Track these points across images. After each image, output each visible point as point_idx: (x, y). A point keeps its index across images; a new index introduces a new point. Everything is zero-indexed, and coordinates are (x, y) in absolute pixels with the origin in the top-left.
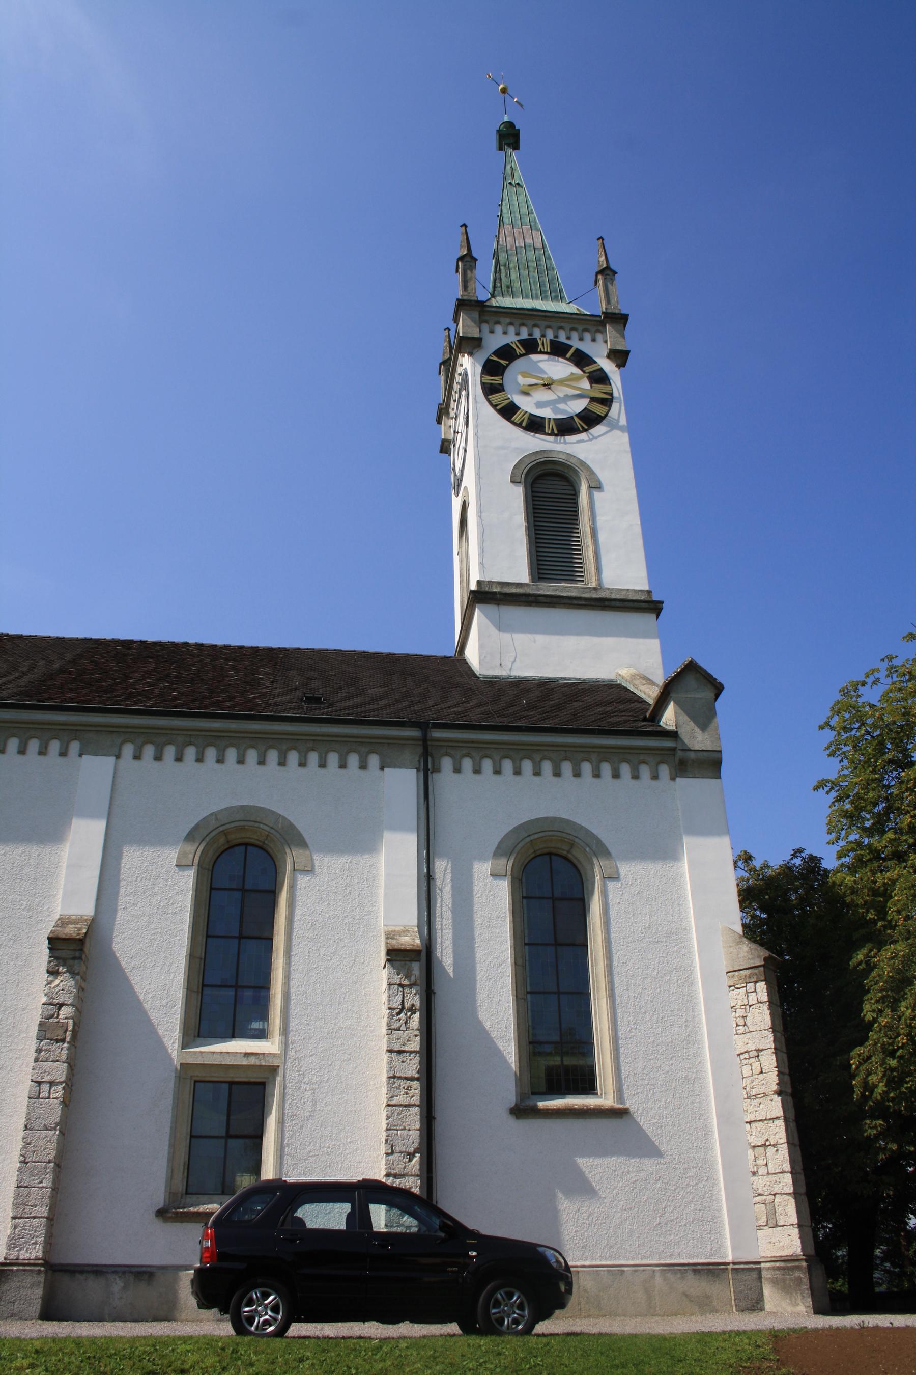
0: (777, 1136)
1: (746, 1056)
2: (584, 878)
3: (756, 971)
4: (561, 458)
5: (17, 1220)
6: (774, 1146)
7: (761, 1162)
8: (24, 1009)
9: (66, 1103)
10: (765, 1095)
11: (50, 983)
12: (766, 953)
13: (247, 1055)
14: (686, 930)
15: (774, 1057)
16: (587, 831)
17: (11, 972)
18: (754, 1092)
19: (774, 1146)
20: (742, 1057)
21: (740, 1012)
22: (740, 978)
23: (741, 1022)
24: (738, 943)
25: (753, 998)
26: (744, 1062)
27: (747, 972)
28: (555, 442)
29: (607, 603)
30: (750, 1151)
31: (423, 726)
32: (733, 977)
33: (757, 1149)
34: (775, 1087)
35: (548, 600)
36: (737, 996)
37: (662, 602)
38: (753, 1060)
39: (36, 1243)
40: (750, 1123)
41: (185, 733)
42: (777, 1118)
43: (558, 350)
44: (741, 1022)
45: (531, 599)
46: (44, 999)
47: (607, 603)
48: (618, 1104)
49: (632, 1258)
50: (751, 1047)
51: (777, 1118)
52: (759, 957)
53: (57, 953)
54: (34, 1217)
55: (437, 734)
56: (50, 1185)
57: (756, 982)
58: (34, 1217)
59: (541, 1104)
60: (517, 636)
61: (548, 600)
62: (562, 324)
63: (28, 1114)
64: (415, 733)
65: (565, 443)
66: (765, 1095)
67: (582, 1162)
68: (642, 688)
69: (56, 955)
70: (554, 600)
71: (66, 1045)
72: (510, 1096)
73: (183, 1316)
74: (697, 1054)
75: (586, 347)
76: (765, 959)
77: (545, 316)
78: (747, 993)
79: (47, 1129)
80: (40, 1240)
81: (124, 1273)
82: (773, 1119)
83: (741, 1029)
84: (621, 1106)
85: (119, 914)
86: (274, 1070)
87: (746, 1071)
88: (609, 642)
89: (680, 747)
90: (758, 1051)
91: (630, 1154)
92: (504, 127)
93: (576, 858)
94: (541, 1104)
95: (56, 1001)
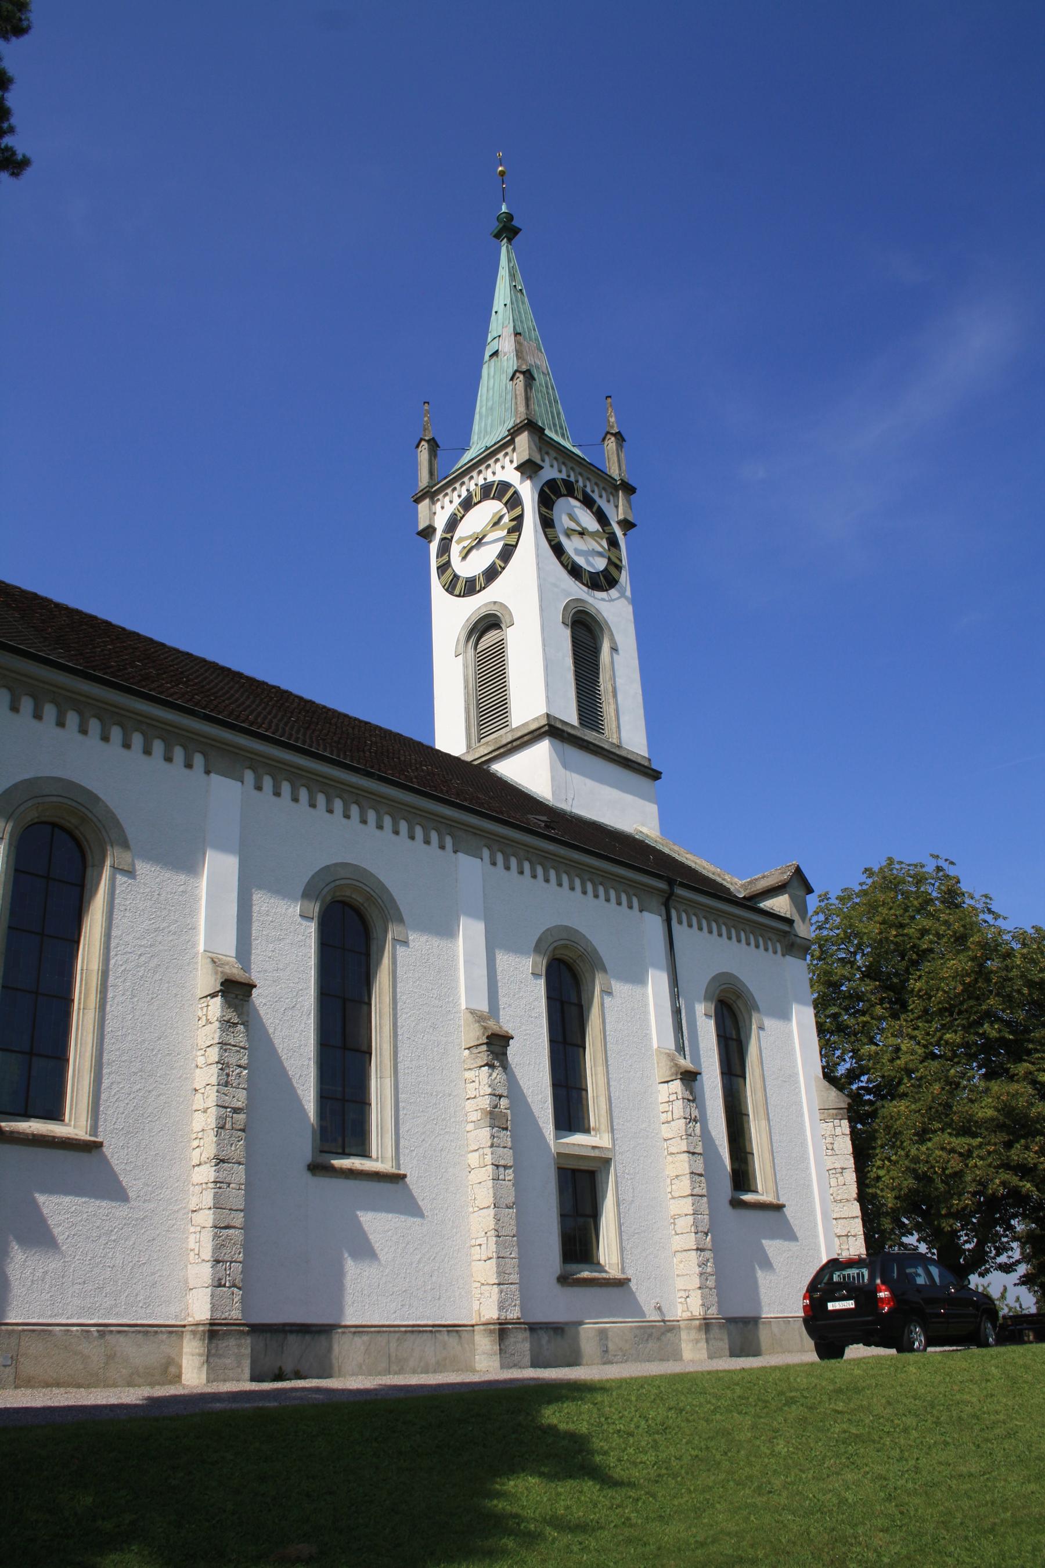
0: (856, 1230)
1: (834, 1171)
2: (740, 1025)
3: (841, 1111)
4: (593, 611)
5: (502, 1286)
6: (854, 1236)
7: (844, 1247)
8: (450, 1095)
9: (516, 1184)
10: (848, 1201)
11: (490, 1075)
12: (850, 1101)
13: (594, 1148)
14: (797, 1074)
15: (854, 1174)
16: (747, 987)
17: (435, 1058)
18: (839, 1198)
19: (854, 1236)
20: (831, 1172)
21: (829, 1140)
22: (829, 1115)
23: (830, 1147)
24: (828, 1089)
25: (838, 1131)
26: (832, 1176)
27: (834, 1111)
28: (588, 593)
29: (630, 763)
30: (836, 1239)
31: (671, 882)
32: (823, 1113)
33: (841, 1238)
34: (855, 1196)
35: (595, 749)
36: (827, 1127)
37: (661, 773)
38: (838, 1175)
39: (515, 1306)
40: (836, 1219)
41: (526, 848)
42: (857, 1217)
43: (588, 502)
44: (830, 1147)
45: (585, 744)
46: (489, 1091)
47: (630, 763)
48: (90, 1135)
49: (791, 1312)
50: (837, 1165)
51: (857, 1217)
52: (844, 1101)
53: (493, 1048)
54: (511, 1284)
55: (680, 891)
56: (517, 1256)
57: (841, 1119)
58: (511, 1284)
59: (339, 1163)
60: (574, 775)
61: (595, 749)
62: (590, 476)
63: (494, 1194)
64: (662, 885)
65: (594, 597)
66: (848, 1201)
67: (764, 1241)
68: (688, 856)
69: (492, 1049)
70: (599, 750)
71: (509, 1133)
72: (304, 1148)
73: (584, 1362)
74: (808, 1168)
75: (608, 509)
76: (849, 1104)
77: (581, 463)
78: (834, 1127)
79: (508, 1208)
80: (518, 1302)
81: (547, 1328)
82: (854, 1218)
83: (830, 1152)
84: (93, 1139)
85: (501, 1013)
86: (607, 1162)
87: (833, 1182)
88: (629, 798)
89: (793, 932)
90: (843, 1169)
91: (785, 1239)
92: (506, 218)
93: (739, 1008)
94: (339, 1163)
95: (497, 1093)
